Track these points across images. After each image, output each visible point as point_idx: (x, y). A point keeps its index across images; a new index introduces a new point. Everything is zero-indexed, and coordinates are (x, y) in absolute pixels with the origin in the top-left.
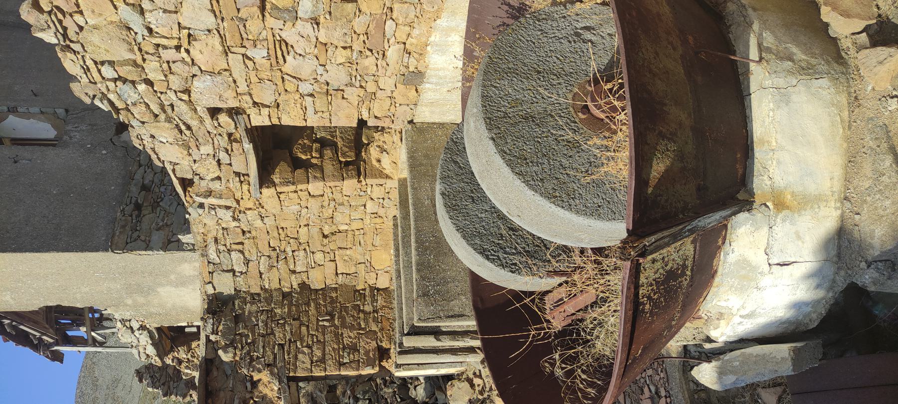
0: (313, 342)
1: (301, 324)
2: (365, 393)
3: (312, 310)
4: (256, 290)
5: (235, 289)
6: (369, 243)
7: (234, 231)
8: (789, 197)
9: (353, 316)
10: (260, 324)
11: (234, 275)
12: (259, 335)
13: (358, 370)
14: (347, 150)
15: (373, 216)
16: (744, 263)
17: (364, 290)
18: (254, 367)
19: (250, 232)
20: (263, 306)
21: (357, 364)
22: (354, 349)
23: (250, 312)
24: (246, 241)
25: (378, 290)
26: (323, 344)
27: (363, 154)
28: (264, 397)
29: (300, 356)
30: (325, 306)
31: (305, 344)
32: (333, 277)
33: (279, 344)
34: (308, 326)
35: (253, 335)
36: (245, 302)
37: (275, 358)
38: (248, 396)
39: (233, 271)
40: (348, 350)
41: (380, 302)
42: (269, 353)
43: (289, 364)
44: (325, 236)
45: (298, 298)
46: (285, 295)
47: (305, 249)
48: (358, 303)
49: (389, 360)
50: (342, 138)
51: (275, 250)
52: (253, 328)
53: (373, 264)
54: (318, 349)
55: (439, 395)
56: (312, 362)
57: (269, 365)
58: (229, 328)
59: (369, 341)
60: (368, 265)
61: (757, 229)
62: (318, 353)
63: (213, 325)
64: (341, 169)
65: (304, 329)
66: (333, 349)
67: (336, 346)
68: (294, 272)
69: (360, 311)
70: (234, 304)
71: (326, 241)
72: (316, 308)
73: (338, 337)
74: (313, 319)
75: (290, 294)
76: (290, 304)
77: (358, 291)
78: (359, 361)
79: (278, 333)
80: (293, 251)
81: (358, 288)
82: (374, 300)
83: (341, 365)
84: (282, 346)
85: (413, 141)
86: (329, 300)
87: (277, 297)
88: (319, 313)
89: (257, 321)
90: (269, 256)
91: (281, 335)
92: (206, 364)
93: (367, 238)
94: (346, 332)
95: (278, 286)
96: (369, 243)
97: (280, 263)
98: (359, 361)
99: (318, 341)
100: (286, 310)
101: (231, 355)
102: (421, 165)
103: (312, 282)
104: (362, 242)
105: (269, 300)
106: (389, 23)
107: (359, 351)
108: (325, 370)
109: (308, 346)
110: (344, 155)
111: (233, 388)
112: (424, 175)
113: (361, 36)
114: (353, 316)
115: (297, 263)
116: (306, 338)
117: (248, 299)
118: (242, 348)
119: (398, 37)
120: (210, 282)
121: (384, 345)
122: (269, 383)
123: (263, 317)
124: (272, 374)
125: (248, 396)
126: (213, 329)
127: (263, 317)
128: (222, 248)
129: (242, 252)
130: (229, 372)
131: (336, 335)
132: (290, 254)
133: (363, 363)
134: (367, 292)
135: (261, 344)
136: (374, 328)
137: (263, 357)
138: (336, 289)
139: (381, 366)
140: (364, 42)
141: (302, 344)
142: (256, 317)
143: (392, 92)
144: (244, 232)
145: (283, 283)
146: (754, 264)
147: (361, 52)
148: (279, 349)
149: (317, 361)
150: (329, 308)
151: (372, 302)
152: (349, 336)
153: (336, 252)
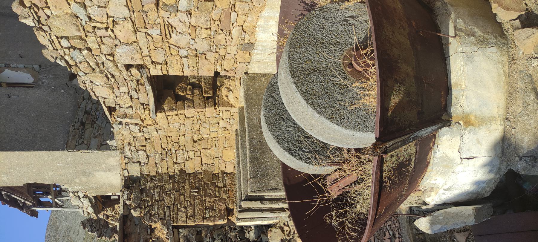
0: (187, 205)
1: (181, 194)
2: (219, 235)
3: (187, 186)
4: (153, 173)
5: (141, 173)
6: (221, 145)
7: (140, 138)
8: (473, 118)
9: (211, 189)
10: (156, 194)
11: (140, 165)
12: (155, 201)
13: (214, 221)
14: (208, 90)
15: (223, 129)
16: (446, 158)
17: (218, 173)
18: (152, 220)
19: (150, 139)
20: (157, 183)
21: (214, 218)
22: (212, 209)
23: (150, 187)
24: (147, 145)
25: (227, 173)
26: (194, 206)
27: (218, 92)
28: (158, 238)
29: (180, 213)
30: (195, 183)
31: (182, 206)
32: (200, 166)
33: (167, 206)
34: (184, 196)
35: (152, 201)
36: (147, 181)
37: (165, 214)
38: (149, 237)
39: (139, 162)
40: (208, 210)
41: (228, 181)
42: (161, 211)
43: (173, 218)
44: (195, 142)
45: (178, 179)
46: (171, 177)
47: (183, 149)
48: (215, 181)
49: (233, 216)
50: (205, 82)
51: (165, 150)
52: (151, 197)
53: (223, 158)
54: (190, 209)
55: (263, 236)
56: (187, 217)
57: (161, 219)
58: (137, 197)
59: (221, 204)
60: (221, 159)
61: (454, 137)
62: (191, 212)
63: (128, 195)
64: (204, 101)
65: (182, 197)
66: (200, 209)
67: (201, 208)
68: (176, 163)
69: (216, 186)
70: (140, 182)
71: (195, 144)
72: (190, 185)
73: (202, 202)
74: (188, 191)
75: (173, 176)
76: (174, 182)
77: (215, 174)
78: (215, 216)
79: (167, 200)
80: (176, 151)
81: (215, 172)
82: (224, 180)
83: (205, 218)
84: (169, 207)
85: (247, 85)
86: (197, 180)
87: (166, 178)
88: (191, 188)
89: (154, 192)
90: (161, 154)
91: (169, 201)
92: (124, 218)
93: (220, 142)
94: (207, 199)
95: (166, 171)
96: (221, 145)
97: (168, 157)
98: (215, 216)
99: (191, 204)
100: (172, 186)
101: (138, 213)
102: (252, 99)
103: (187, 169)
104: (217, 145)
105: (161, 180)
106: (233, 14)
107: (215, 210)
108: (195, 221)
109: (185, 208)
110: (206, 93)
111: (140, 232)
112: (254, 105)
113: (217, 22)
114: (211, 189)
115: (178, 157)
116: (183, 203)
117: (149, 179)
118: (145, 208)
119: (238, 22)
120: (126, 169)
121: (230, 206)
122: (161, 229)
123: (158, 190)
124: (163, 224)
125: (149, 237)
126: (128, 197)
127: (158, 190)
128: (133, 148)
129: (145, 151)
130: (137, 223)
131: (202, 201)
132: (174, 152)
133: (218, 217)
134: (220, 175)
135: (157, 206)
136: (224, 196)
137: (158, 214)
138: (201, 173)
139: (228, 219)
140: (218, 25)
141: (181, 206)
142: (153, 190)
143: (235, 55)
144: (146, 139)
145: (169, 169)
146: (451, 158)
147: (216, 31)
148: (167, 209)
149: (190, 217)
150: (197, 185)
151: (223, 181)
152: (209, 202)
153: (202, 151)
